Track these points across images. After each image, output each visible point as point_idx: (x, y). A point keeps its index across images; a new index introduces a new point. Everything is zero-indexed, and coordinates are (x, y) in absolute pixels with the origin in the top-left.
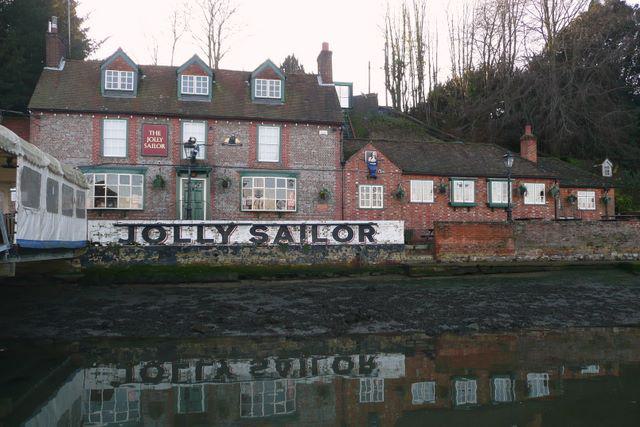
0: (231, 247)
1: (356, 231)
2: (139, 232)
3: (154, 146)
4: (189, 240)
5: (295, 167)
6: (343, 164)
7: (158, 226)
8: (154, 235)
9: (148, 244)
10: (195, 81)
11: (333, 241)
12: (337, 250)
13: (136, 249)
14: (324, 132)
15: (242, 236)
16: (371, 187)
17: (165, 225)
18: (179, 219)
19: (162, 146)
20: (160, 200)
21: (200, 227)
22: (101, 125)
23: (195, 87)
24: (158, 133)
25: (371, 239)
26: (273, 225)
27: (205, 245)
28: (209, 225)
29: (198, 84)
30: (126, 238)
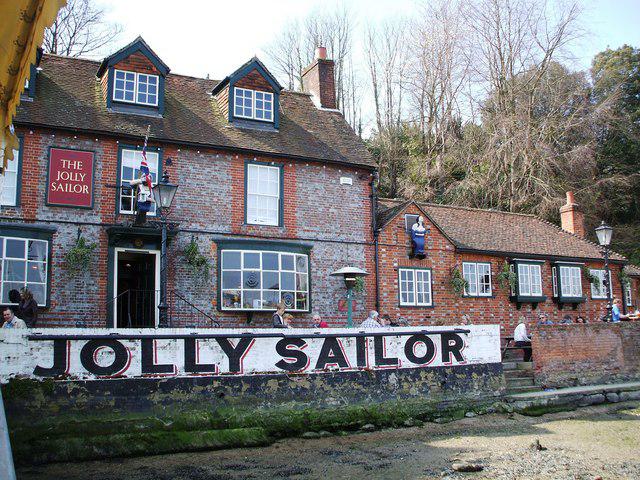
0: (247, 379)
1: (437, 340)
2: (75, 350)
3: (69, 189)
4: (170, 368)
5: (305, 235)
6: (375, 234)
7: (111, 341)
8: (105, 358)
9: (92, 378)
10: (254, 99)
11: (406, 364)
12: (413, 377)
13: (70, 388)
14: (347, 180)
15: (262, 358)
16: (415, 272)
17: (340, 336)
18: (152, 325)
19: (85, 189)
20: (79, 287)
21: (190, 343)
22: (246, 167)
23: (136, 92)
24: (77, 165)
25: (459, 357)
26: (317, 336)
27: (201, 375)
28: (205, 337)
29: (259, 104)
30: (49, 364)
